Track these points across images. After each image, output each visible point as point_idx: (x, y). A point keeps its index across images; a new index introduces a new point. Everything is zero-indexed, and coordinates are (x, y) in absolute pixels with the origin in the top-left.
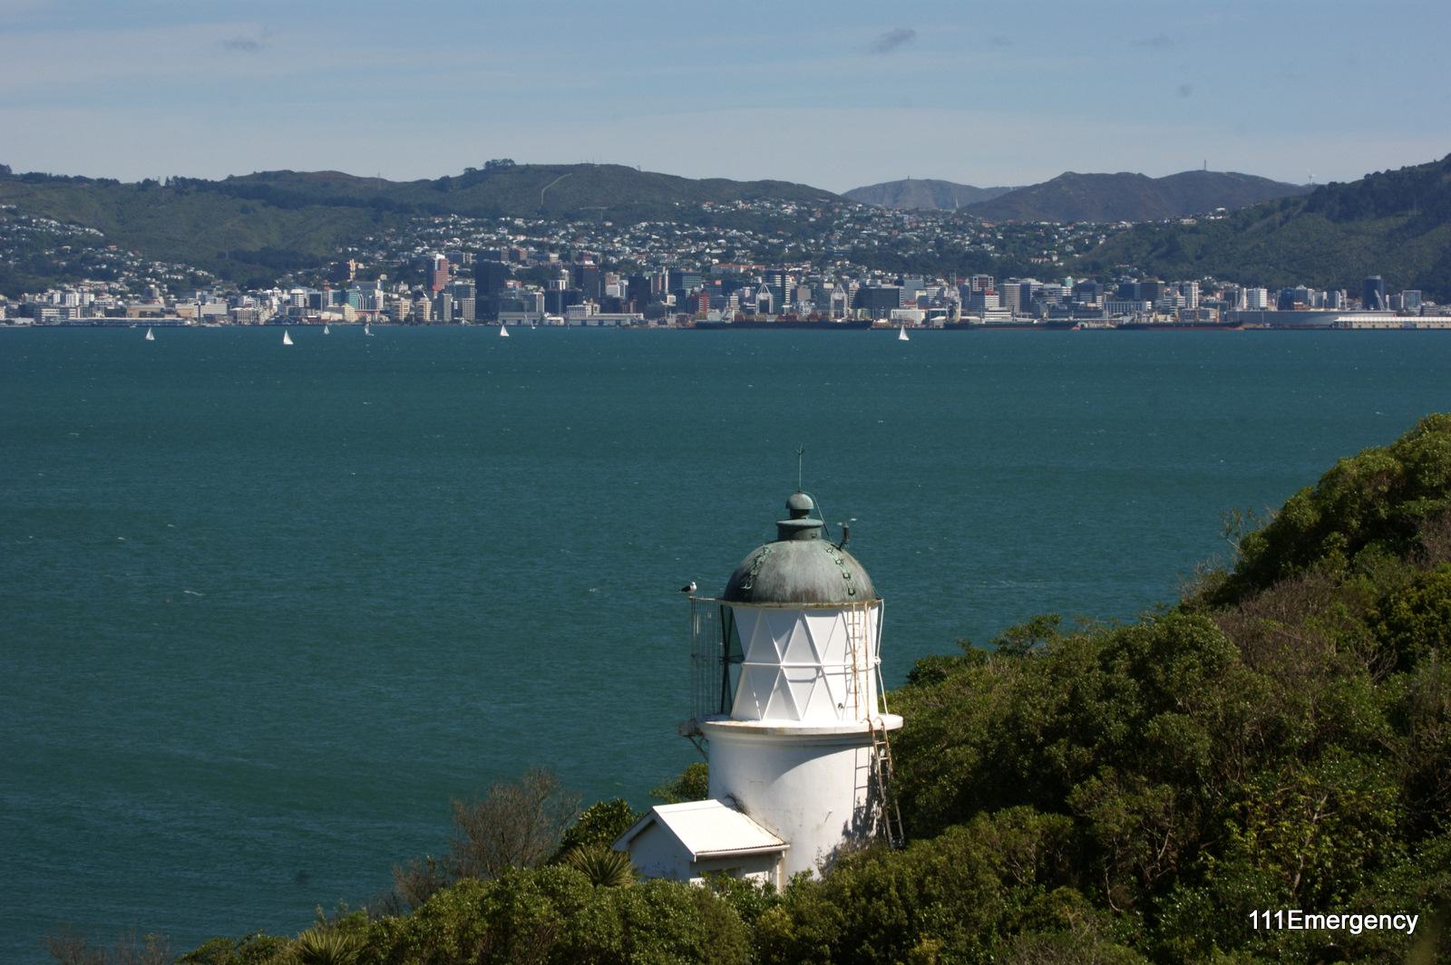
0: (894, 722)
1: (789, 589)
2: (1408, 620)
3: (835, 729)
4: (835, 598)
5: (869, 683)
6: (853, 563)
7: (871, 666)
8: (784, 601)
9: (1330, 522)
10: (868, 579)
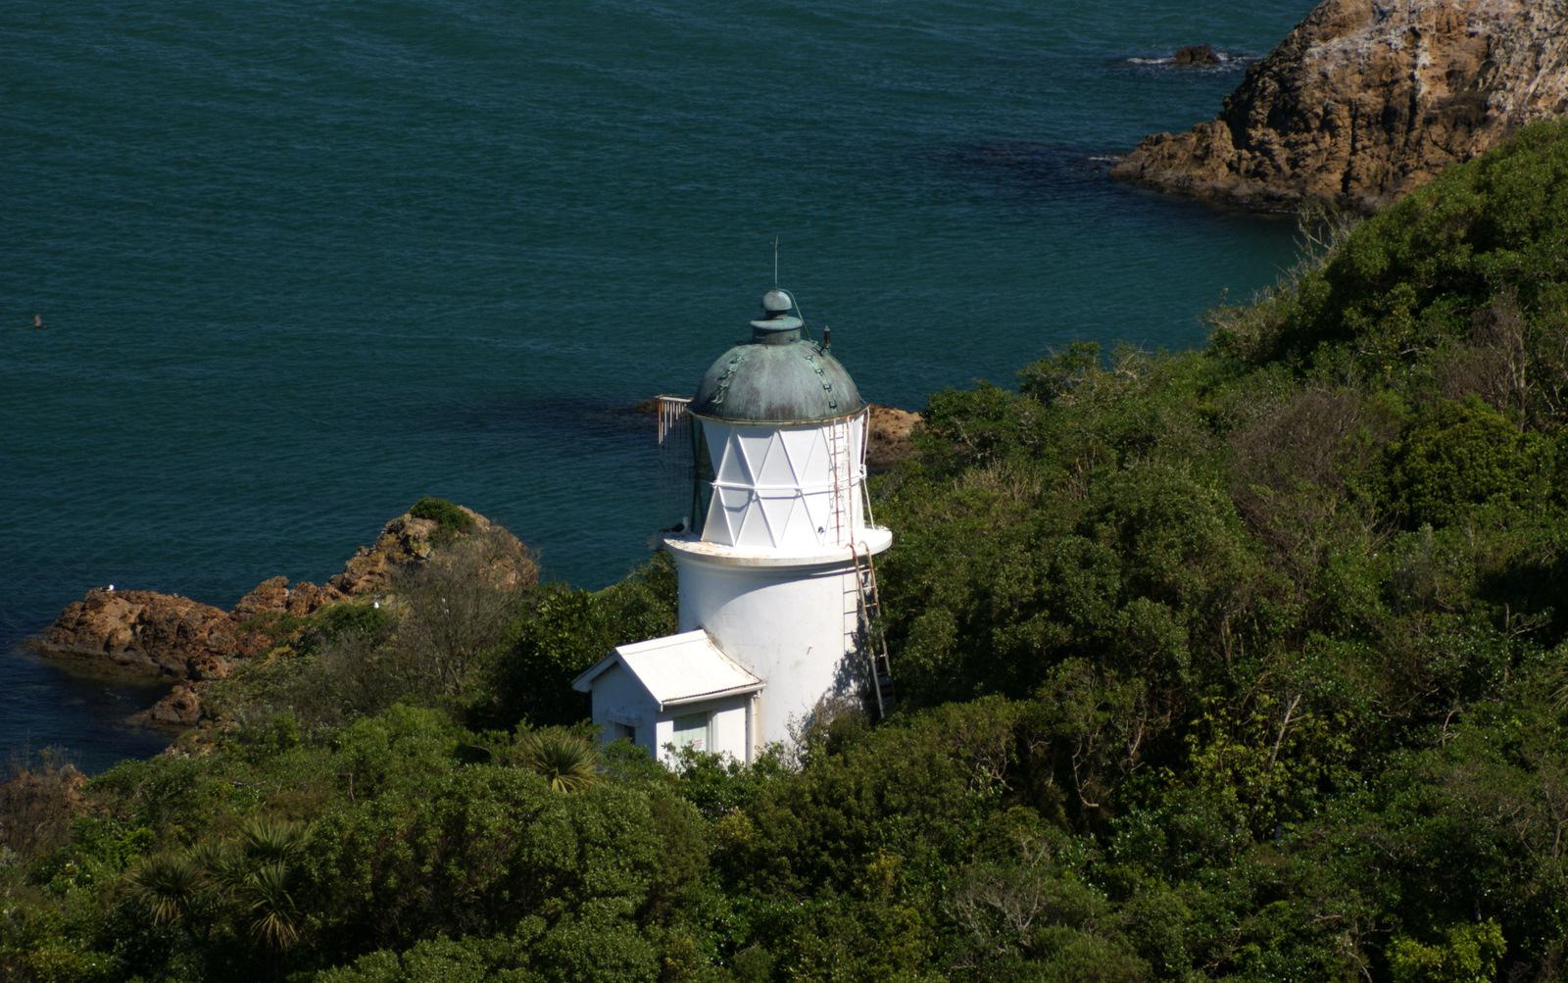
0: (879, 539)
1: (763, 405)
2: (1421, 471)
3: (815, 558)
4: (813, 413)
5: (854, 501)
6: (834, 369)
7: (855, 481)
8: (757, 419)
9: (1398, 270)
10: (851, 382)
